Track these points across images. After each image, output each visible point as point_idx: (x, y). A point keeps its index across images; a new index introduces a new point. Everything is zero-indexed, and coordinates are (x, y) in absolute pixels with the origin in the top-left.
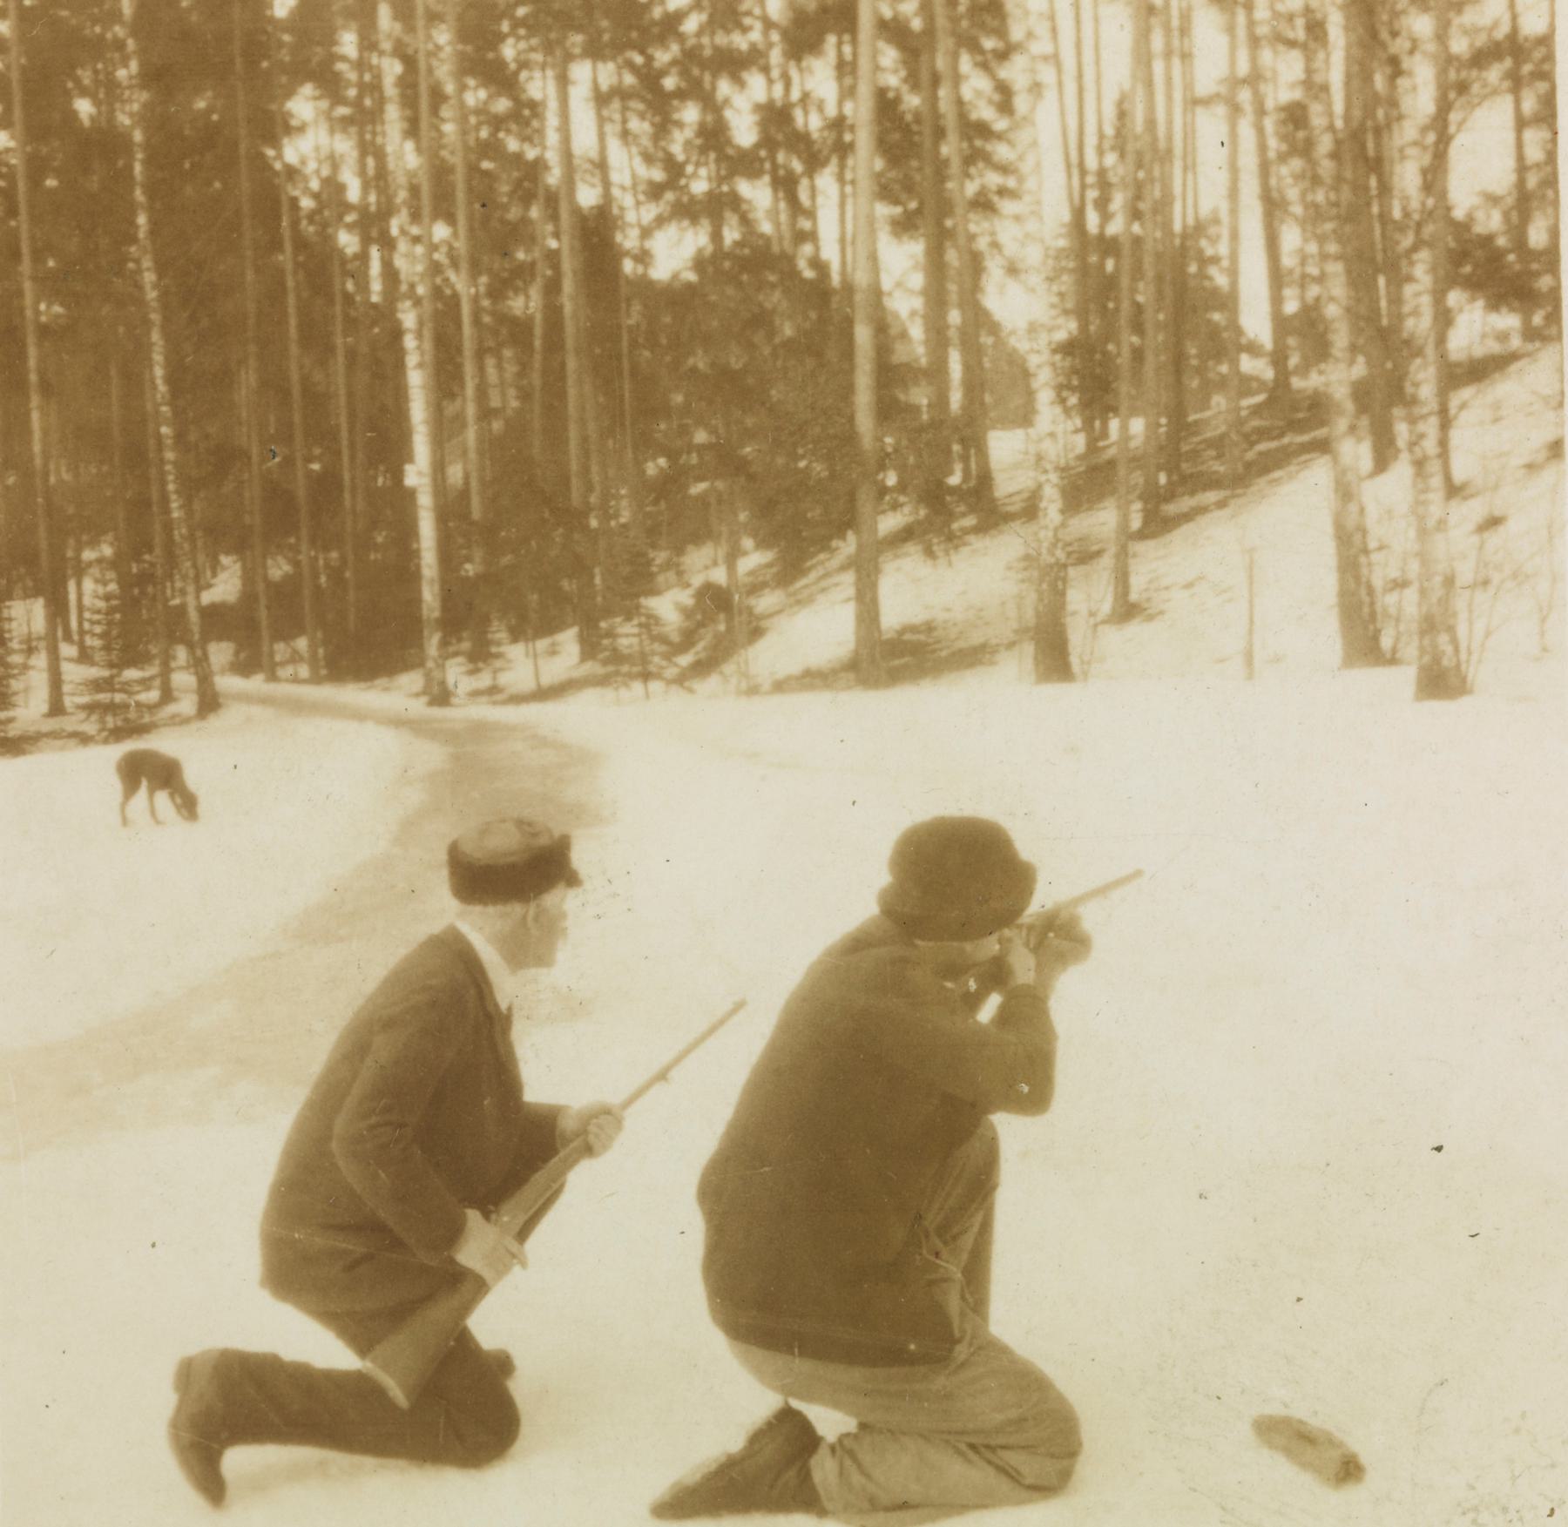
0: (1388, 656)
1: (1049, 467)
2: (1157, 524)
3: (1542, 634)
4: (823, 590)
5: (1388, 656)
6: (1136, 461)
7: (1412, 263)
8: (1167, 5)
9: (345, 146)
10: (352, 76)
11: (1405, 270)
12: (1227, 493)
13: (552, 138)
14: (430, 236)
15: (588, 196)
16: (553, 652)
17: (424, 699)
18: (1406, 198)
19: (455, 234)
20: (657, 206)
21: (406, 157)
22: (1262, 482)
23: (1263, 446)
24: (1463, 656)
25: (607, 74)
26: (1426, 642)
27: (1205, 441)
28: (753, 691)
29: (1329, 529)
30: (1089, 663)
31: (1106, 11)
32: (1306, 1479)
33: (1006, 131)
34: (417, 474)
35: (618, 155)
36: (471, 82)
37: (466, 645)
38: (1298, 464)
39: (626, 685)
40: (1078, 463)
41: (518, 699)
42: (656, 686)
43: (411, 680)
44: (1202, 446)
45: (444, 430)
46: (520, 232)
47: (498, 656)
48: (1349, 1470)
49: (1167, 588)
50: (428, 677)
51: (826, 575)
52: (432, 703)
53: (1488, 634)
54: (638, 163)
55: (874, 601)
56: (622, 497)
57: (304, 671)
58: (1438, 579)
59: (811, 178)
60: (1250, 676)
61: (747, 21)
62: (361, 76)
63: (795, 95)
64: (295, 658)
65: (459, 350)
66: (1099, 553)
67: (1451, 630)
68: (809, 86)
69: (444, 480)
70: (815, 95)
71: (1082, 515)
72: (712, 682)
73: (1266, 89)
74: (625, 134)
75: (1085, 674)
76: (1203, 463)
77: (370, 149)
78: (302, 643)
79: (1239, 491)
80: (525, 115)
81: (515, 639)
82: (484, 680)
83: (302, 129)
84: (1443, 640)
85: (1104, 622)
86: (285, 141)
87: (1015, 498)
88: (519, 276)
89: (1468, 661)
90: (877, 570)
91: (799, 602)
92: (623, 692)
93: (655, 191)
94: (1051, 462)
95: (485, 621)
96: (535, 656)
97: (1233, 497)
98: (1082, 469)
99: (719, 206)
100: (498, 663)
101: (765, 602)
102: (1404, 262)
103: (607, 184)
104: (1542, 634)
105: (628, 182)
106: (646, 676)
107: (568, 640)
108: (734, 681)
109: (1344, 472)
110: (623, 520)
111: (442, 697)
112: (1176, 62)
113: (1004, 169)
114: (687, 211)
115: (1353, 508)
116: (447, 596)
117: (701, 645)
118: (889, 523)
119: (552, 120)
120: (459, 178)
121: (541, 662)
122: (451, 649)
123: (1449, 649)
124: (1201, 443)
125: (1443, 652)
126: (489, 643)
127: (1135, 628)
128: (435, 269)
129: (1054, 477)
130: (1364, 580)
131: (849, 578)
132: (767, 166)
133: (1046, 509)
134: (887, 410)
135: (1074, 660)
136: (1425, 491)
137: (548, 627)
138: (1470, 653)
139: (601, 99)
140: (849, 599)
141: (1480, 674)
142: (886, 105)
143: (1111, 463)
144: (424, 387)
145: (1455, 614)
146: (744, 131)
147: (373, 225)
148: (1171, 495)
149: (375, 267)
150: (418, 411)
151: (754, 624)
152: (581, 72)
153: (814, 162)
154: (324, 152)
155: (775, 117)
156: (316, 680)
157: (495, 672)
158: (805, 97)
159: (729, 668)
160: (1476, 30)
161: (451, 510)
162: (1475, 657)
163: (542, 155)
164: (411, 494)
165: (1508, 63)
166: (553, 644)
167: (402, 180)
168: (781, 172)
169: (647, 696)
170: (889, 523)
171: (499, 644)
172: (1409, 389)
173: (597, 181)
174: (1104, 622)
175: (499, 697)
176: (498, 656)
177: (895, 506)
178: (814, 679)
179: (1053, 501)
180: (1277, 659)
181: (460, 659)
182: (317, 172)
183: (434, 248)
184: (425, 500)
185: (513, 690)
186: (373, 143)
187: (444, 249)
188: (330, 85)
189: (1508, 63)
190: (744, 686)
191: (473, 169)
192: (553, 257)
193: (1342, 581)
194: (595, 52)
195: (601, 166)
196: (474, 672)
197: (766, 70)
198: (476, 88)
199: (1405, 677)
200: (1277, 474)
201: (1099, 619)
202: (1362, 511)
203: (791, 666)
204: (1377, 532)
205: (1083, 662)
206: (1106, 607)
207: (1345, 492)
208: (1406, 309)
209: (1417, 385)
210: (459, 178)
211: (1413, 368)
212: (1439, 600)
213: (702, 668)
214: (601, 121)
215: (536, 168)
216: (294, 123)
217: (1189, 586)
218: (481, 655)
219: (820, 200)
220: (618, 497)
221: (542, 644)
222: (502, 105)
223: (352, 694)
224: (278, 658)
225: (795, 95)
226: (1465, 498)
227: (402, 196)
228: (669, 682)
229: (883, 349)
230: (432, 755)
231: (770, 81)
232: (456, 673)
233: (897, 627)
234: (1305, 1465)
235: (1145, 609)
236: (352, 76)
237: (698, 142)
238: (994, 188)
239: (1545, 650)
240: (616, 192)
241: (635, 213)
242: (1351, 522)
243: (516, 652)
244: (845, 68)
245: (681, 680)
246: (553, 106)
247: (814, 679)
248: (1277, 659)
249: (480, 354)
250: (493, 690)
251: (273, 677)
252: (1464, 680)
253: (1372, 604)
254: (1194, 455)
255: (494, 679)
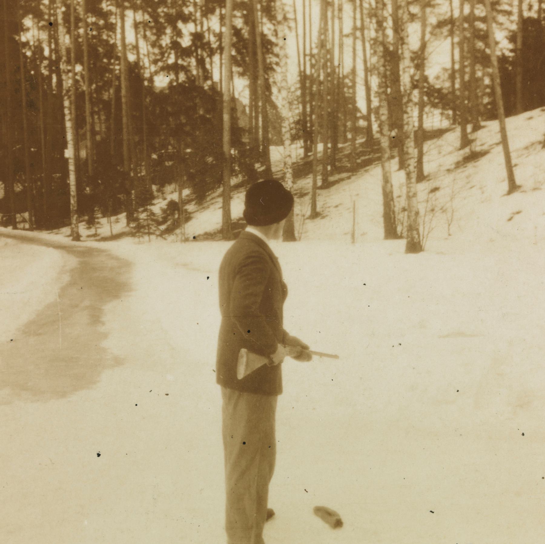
0: (399, 235)
1: (288, 167)
2: (327, 185)
3: (449, 230)
4: (212, 204)
5: (399, 235)
6: (319, 161)
7: (407, 107)
8: (333, 1)
9: (44, 36)
10: (47, 11)
11: (404, 109)
12: (350, 174)
13: (119, 36)
14: (74, 70)
15: (132, 58)
16: (117, 221)
17: (71, 238)
18: (405, 85)
19: (83, 70)
20: (155, 67)
21: (65, 40)
22: (362, 170)
23: (363, 158)
24: (421, 238)
25: (140, 16)
26: (409, 234)
27: (344, 155)
28: (187, 240)
29: (380, 191)
30: (301, 233)
31: (314, 3)
32: (327, 526)
33: (290, 19)
34: (69, 153)
35: (142, 44)
36: (90, 15)
37: (86, 218)
38: (375, 164)
39: (142, 237)
40: (302, 161)
41: (105, 239)
42: (153, 237)
43: (66, 230)
44: (343, 157)
45: (78, 139)
46: (106, 69)
47: (98, 223)
48: (338, 524)
49: (329, 207)
50: (72, 229)
51: (213, 199)
52: (73, 240)
53: (429, 232)
54: (150, 47)
55: (229, 210)
56: (143, 166)
57: (27, 226)
58: (413, 213)
59: (211, 58)
60: (353, 242)
61: (188, 4)
62: (50, 11)
63: (205, 28)
64: (24, 221)
65: (85, 112)
66: (306, 194)
67: (417, 230)
68: (210, 25)
69: (79, 155)
70: (212, 28)
71: (302, 180)
72: (171, 238)
73: (366, 32)
74: (145, 37)
75: (300, 238)
76: (343, 163)
77: (54, 38)
78: (26, 215)
79: (354, 174)
80: (111, 27)
81: (104, 216)
82: (92, 231)
83: (28, 29)
84: (415, 232)
85: (307, 218)
86: (22, 33)
87: (278, 173)
88: (108, 84)
89: (423, 240)
90: (231, 198)
91: (204, 208)
92: (141, 239)
93: (155, 62)
94: (289, 165)
95: (93, 211)
96: (111, 223)
97: (353, 175)
98: (301, 163)
99: (175, 68)
100: (98, 226)
101: (191, 207)
102: (404, 106)
103: (138, 53)
104: (449, 230)
105: (146, 53)
106: (149, 234)
107: (123, 217)
108: (180, 236)
109: (386, 173)
110: (143, 174)
111: (77, 237)
112: (337, 21)
113: (277, 56)
114: (167, 69)
115: (389, 185)
116: (79, 202)
117: (169, 223)
118: (234, 181)
119: (119, 31)
120: (84, 48)
121: (112, 225)
122: (81, 219)
123: (417, 236)
124: (342, 155)
125: (415, 237)
126: (95, 218)
127: (318, 221)
128: (76, 82)
129: (290, 170)
130: (392, 209)
131: (220, 200)
132: (195, 54)
133: (287, 181)
134: (236, 142)
135: (296, 234)
136: (411, 183)
137: (115, 212)
138: (423, 238)
139: (136, 25)
140: (220, 208)
141: (427, 244)
142: (237, 32)
143: (311, 161)
144: (71, 128)
145: (419, 224)
146: (186, 42)
147: (54, 66)
148: (332, 174)
149: (54, 79)
150: (69, 136)
151: (188, 215)
152: (129, 14)
153: (212, 53)
154: (36, 37)
155: (197, 37)
156: (31, 229)
157: (96, 228)
158: (209, 29)
159: (178, 231)
160: (440, 14)
161: (80, 165)
162: (425, 239)
163: (115, 42)
164: (67, 160)
165: (449, 26)
166: (117, 219)
167: (64, 47)
168: (199, 57)
169: (150, 241)
170: (234, 181)
171: (98, 218)
172: (405, 149)
173: (135, 52)
174: (307, 218)
175: (98, 238)
176: (98, 223)
177: (237, 176)
178: (209, 236)
179: (290, 179)
180: (363, 234)
181: (84, 223)
182: (34, 45)
183: (76, 74)
184: (71, 162)
185: (102, 235)
186: (54, 35)
187: (79, 75)
188: (38, 15)
189: (449, 26)
190: (183, 238)
191: (89, 45)
192: (118, 78)
193: (385, 209)
194: (135, 8)
195: (136, 47)
196: (89, 228)
197: (195, 21)
198: (92, 17)
199: (402, 244)
200: (367, 168)
201: (305, 217)
202: (392, 186)
203: (199, 231)
204: (396, 193)
205: (299, 233)
206: (308, 213)
207: (386, 180)
208: (405, 122)
209: (407, 148)
210: (84, 48)
211: (406, 142)
212: (414, 220)
213: (169, 231)
214: (137, 33)
215: (114, 46)
216: (25, 28)
217: (337, 206)
218: (91, 222)
219: (214, 65)
220: (141, 165)
221: (113, 218)
222: (102, 22)
223: (44, 235)
224: (17, 220)
225: (205, 28)
226: (429, 180)
227: (64, 52)
228: (157, 236)
229: (234, 119)
230: (73, 261)
231: (196, 25)
232: (83, 230)
233: (238, 218)
234: (327, 522)
235: (322, 214)
236: (47, 11)
237: (170, 45)
238: (274, 62)
239: (450, 235)
240: (141, 56)
241: (149, 69)
242: (388, 190)
243: (104, 221)
244: (222, 18)
245: (162, 234)
246: (119, 24)
247: (209, 236)
248: (363, 234)
249: (92, 114)
250: (95, 235)
251: (15, 228)
252: (421, 247)
253: (395, 217)
254: (340, 160)
255: (96, 231)
